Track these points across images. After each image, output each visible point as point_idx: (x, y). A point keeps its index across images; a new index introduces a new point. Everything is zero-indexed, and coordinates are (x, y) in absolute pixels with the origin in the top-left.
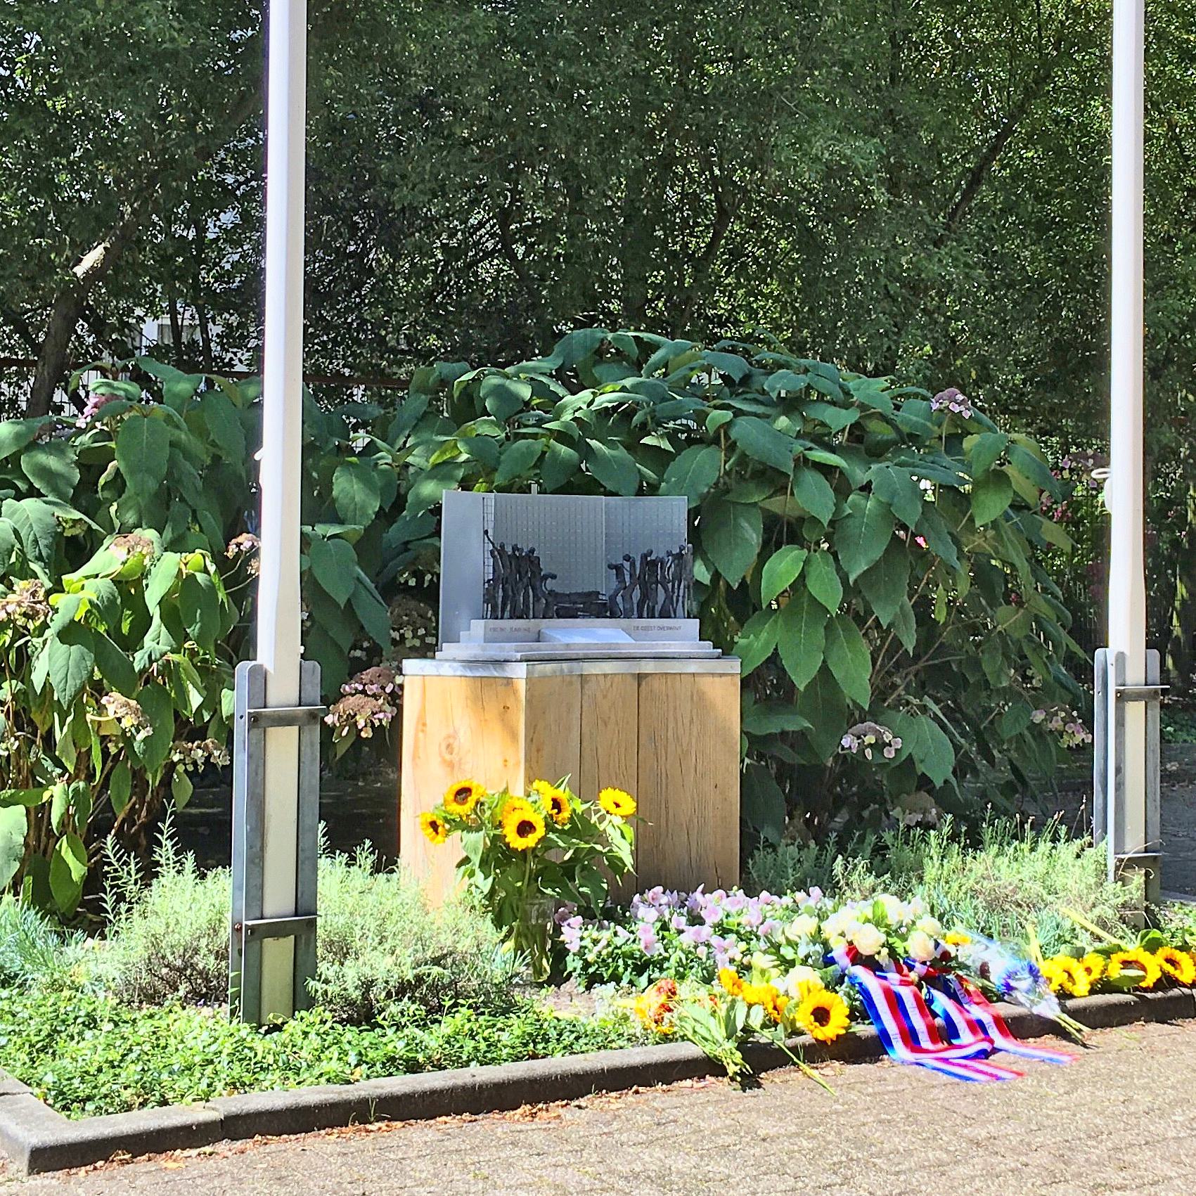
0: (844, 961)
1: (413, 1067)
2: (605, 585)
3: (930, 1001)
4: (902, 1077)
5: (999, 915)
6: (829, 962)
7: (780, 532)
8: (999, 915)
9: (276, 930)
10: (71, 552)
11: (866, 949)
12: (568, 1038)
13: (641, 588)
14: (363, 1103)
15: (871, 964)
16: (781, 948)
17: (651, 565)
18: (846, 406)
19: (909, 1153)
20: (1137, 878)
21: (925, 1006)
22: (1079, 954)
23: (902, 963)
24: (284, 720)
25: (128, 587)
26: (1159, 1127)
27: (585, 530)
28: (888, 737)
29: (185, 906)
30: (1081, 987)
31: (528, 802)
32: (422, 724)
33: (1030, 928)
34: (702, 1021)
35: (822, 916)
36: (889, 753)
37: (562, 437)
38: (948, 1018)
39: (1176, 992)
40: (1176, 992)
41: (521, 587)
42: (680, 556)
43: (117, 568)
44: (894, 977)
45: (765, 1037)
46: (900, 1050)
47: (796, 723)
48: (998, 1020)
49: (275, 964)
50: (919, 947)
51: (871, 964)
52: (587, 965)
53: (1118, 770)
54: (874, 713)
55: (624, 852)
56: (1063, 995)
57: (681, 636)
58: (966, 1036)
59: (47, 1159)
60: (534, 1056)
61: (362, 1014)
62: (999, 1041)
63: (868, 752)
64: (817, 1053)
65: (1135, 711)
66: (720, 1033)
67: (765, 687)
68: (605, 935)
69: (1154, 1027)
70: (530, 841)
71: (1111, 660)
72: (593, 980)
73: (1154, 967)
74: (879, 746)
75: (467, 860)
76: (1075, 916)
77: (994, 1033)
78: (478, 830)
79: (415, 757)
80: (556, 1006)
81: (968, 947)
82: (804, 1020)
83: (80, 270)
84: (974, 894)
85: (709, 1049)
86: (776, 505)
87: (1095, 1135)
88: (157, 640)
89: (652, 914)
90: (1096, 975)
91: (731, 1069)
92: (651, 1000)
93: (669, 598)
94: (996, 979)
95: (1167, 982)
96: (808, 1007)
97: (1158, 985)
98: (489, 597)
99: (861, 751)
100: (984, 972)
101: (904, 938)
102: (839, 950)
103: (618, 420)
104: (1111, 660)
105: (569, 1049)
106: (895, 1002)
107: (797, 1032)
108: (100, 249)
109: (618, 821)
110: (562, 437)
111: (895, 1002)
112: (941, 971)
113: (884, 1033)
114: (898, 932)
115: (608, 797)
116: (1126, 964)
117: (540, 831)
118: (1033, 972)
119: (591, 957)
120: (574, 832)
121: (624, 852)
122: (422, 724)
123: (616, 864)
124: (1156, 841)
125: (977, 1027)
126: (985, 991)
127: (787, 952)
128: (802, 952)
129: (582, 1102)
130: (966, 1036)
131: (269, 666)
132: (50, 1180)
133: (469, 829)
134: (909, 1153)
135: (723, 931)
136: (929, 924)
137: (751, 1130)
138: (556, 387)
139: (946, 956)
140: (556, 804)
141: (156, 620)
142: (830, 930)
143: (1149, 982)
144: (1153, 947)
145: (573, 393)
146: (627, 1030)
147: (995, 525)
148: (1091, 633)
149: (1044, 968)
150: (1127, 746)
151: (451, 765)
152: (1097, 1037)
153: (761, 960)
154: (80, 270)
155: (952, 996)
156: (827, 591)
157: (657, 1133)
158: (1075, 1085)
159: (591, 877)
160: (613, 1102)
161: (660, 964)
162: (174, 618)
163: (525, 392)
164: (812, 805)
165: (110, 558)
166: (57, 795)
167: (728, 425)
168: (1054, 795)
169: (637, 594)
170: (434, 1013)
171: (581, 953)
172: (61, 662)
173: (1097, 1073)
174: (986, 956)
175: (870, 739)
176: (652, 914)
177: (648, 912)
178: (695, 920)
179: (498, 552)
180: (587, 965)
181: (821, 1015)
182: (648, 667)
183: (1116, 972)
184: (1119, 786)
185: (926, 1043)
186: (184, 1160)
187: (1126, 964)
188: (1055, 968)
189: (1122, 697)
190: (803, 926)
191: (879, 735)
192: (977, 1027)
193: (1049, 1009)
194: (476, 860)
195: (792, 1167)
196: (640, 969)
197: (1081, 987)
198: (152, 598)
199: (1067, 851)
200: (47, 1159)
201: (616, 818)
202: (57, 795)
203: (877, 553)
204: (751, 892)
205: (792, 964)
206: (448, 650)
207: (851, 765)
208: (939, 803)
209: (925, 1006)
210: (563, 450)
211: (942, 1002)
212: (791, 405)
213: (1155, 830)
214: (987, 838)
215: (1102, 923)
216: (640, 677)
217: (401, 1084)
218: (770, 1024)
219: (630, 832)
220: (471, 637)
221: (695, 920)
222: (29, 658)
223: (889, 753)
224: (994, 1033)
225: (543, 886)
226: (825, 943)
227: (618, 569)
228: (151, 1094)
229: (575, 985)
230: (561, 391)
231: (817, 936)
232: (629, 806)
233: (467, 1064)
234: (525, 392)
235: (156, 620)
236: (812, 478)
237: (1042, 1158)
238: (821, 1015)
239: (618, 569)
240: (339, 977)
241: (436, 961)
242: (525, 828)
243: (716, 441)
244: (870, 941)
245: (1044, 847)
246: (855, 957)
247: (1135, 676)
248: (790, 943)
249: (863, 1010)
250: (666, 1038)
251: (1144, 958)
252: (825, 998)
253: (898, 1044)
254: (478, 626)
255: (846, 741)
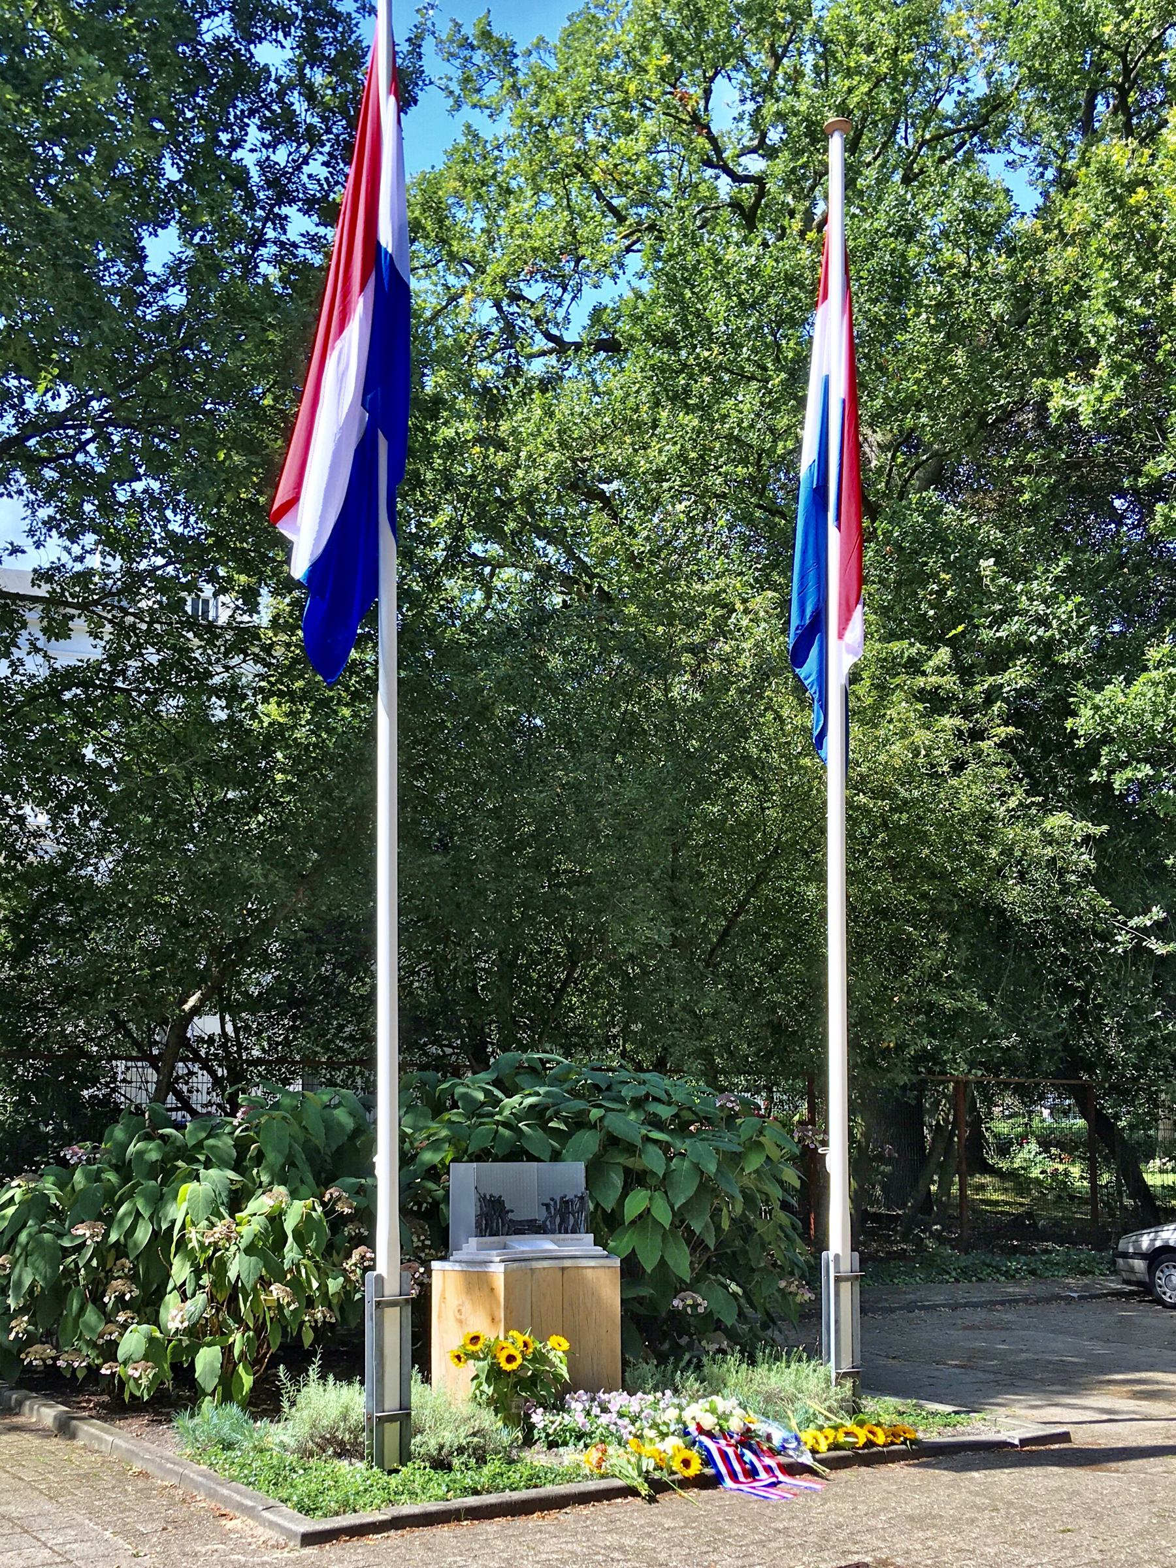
0: (695, 1433)
1: (476, 1492)
2: (540, 1215)
3: (743, 1455)
4: (732, 1497)
5: (772, 1405)
6: (687, 1434)
7: (635, 1179)
8: (772, 1405)
9: (391, 1419)
10: (236, 1200)
11: (707, 1427)
12: (550, 1477)
13: (560, 1217)
14: (458, 1510)
15: (710, 1435)
16: (654, 1424)
17: (566, 1203)
18: (669, 1104)
19: (744, 1536)
20: (849, 1384)
21: (740, 1457)
22: (820, 1428)
23: (726, 1434)
24: (393, 1304)
25: (275, 1219)
26: (872, 1522)
27: (524, 1183)
28: (700, 1300)
29: (325, 1402)
30: (823, 1447)
31: (514, 1345)
32: (443, 1298)
33: (790, 1414)
34: (623, 1465)
35: (681, 1408)
36: (701, 1310)
37: (505, 1124)
38: (752, 1463)
39: (875, 1449)
40: (875, 1449)
41: (496, 1219)
42: (582, 1198)
43: (267, 1209)
44: (723, 1442)
45: (657, 1475)
46: (728, 1483)
47: (646, 1291)
48: (779, 1465)
49: (390, 1439)
50: (735, 1425)
51: (710, 1435)
52: (548, 1435)
53: (837, 1322)
54: (691, 1287)
55: (564, 1371)
56: (814, 1451)
57: (584, 1243)
58: (763, 1475)
59: (309, 1539)
60: (536, 1486)
61: (441, 1464)
62: (782, 1478)
63: (689, 1310)
64: (685, 1484)
65: (846, 1287)
66: (635, 1474)
67: (630, 1270)
68: (559, 1418)
69: (863, 1469)
70: (514, 1366)
71: (831, 1258)
72: (552, 1445)
73: (862, 1436)
74: (695, 1306)
75: (476, 1377)
76: (815, 1406)
77: (778, 1473)
78: (484, 1359)
79: (439, 1317)
80: (538, 1457)
81: (761, 1427)
82: (676, 1465)
83: (187, 1007)
84: (758, 1393)
85: (629, 1482)
86: (630, 1162)
87: (839, 1526)
88: (291, 1252)
89: (579, 1406)
90: (831, 1440)
91: (643, 1493)
92: (593, 1454)
93: (576, 1222)
94: (776, 1442)
95: (870, 1444)
96: (679, 1459)
97: (865, 1446)
98: (478, 1225)
99: (685, 1308)
100: (769, 1438)
101: (727, 1421)
102: (692, 1428)
103: (537, 1114)
104: (831, 1258)
105: (552, 1482)
106: (724, 1456)
107: (673, 1473)
108: (198, 994)
109: (561, 1354)
110: (505, 1124)
111: (724, 1456)
112: (747, 1439)
113: (719, 1473)
114: (725, 1417)
115: (554, 1341)
116: (847, 1434)
117: (519, 1361)
118: (797, 1439)
119: (551, 1431)
120: (534, 1360)
121: (564, 1371)
122: (443, 1298)
123: (557, 1377)
124: (858, 1362)
125: (768, 1469)
126: (770, 1449)
127: (664, 1429)
128: (672, 1429)
129: (567, 1510)
130: (763, 1475)
131: (385, 1275)
132: (311, 1551)
133: (479, 1359)
134: (744, 1536)
135: (621, 1415)
136: (739, 1411)
137: (661, 1525)
138: (497, 1092)
139: (749, 1430)
140: (526, 1345)
141: (290, 1239)
142: (687, 1415)
143: (861, 1444)
144: (861, 1424)
145: (510, 1097)
146: (582, 1472)
147: (756, 1171)
148: (821, 1243)
149: (804, 1436)
150: (840, 1306)
151: (460, 1322)
152: (833, 1475)
153: (650, 1433)
154: (187, 1007)
155: (754, 1452)
156: (664, 1216)
157: (611, 1526)
158: (825, 1501)
159: (546, 1387)
160: (585, 1510)
161: (590, 1435)
162: (300, 1237)
163: (481, 1096)
164: (660, 1340)
165: (260, 1204)
166: (238, 1339)
167: (601, 1119)
168: (787, 1328)
169: (558, 1220)
170: (482, 1461)
171: (544, 1428)
172: (246, 1266)
173: (836, 1494)
174: (770, 1430)
175: (689, 1302)
176: (579, 1406)
177: (577, 1404)
178: (605, 1410)
179: (482, 1199)
180: (548, 1435)
181: (686, 1463)
182: (568, 1263)
183: (842, 1439)
184: (837, 1331)
185: (742, 1479)
186: (374, 1539)
187: (847, 1434)
188: (808, 1436)
189: (838, 1280)
190: (672, 1413)
191: (695, 1300)
192: (768, 1469)
193: (807, 1459)
194: (483, 1377)
195: (686, 1543)
196: (579, 1438)
197: (823, 1447)
198: (289, 1225)
199: (806, 1368)
200: (309, 1539)
201: (557, 1349)
202: (238, 1339)
203: (691, 1193)
204: (631, 1393)
205: (666, 1435)
206: (457, 1255)
207: (675, 1314)
208: (729, 1338)
209: (740, 1457)
210: (507, 1133)
211: (749, 1456)
212: (638, 1103)
213: (858, 1356)
214: (760, 1360)
215: (830, 1409)
216: (563, 1269)
217: (472, 1501)
218: (658, 1468)
219: (565, 1360)
220: (470, 1247)
221: (605, 1410)
222: (225, 1263)
223: (701, 1310)
224: (778, 1473)
225: (519, 1391)
226: (684, 1423)
227: (547, 1206)
228: (346, 1506)
229: (540, 1446)
230: (500, 1095)
231: (680, 1420)
232: (566, 1345)
233: (503, 1490)
234: (481, 1096)
235: (290, 1239)
236: (652, 1149)
237: (813, 1538)
238: (686, 1463)
239: (547, 1206)
240: (426, 1443)
241: (474, 1434)
242: (510, 1359)
243: (594, 1126)
244: (709, 1422)
245: (794, 1366)
246: (700, 1429)
247: (845, 1267)
248: (665, 1423)
249: (708, 1461)
250: (603, 1477)
251: (857, 1430)
252: (687, 1454)
253: (727, 1479)
254: (473, 1241)
255: (676, 1302)
